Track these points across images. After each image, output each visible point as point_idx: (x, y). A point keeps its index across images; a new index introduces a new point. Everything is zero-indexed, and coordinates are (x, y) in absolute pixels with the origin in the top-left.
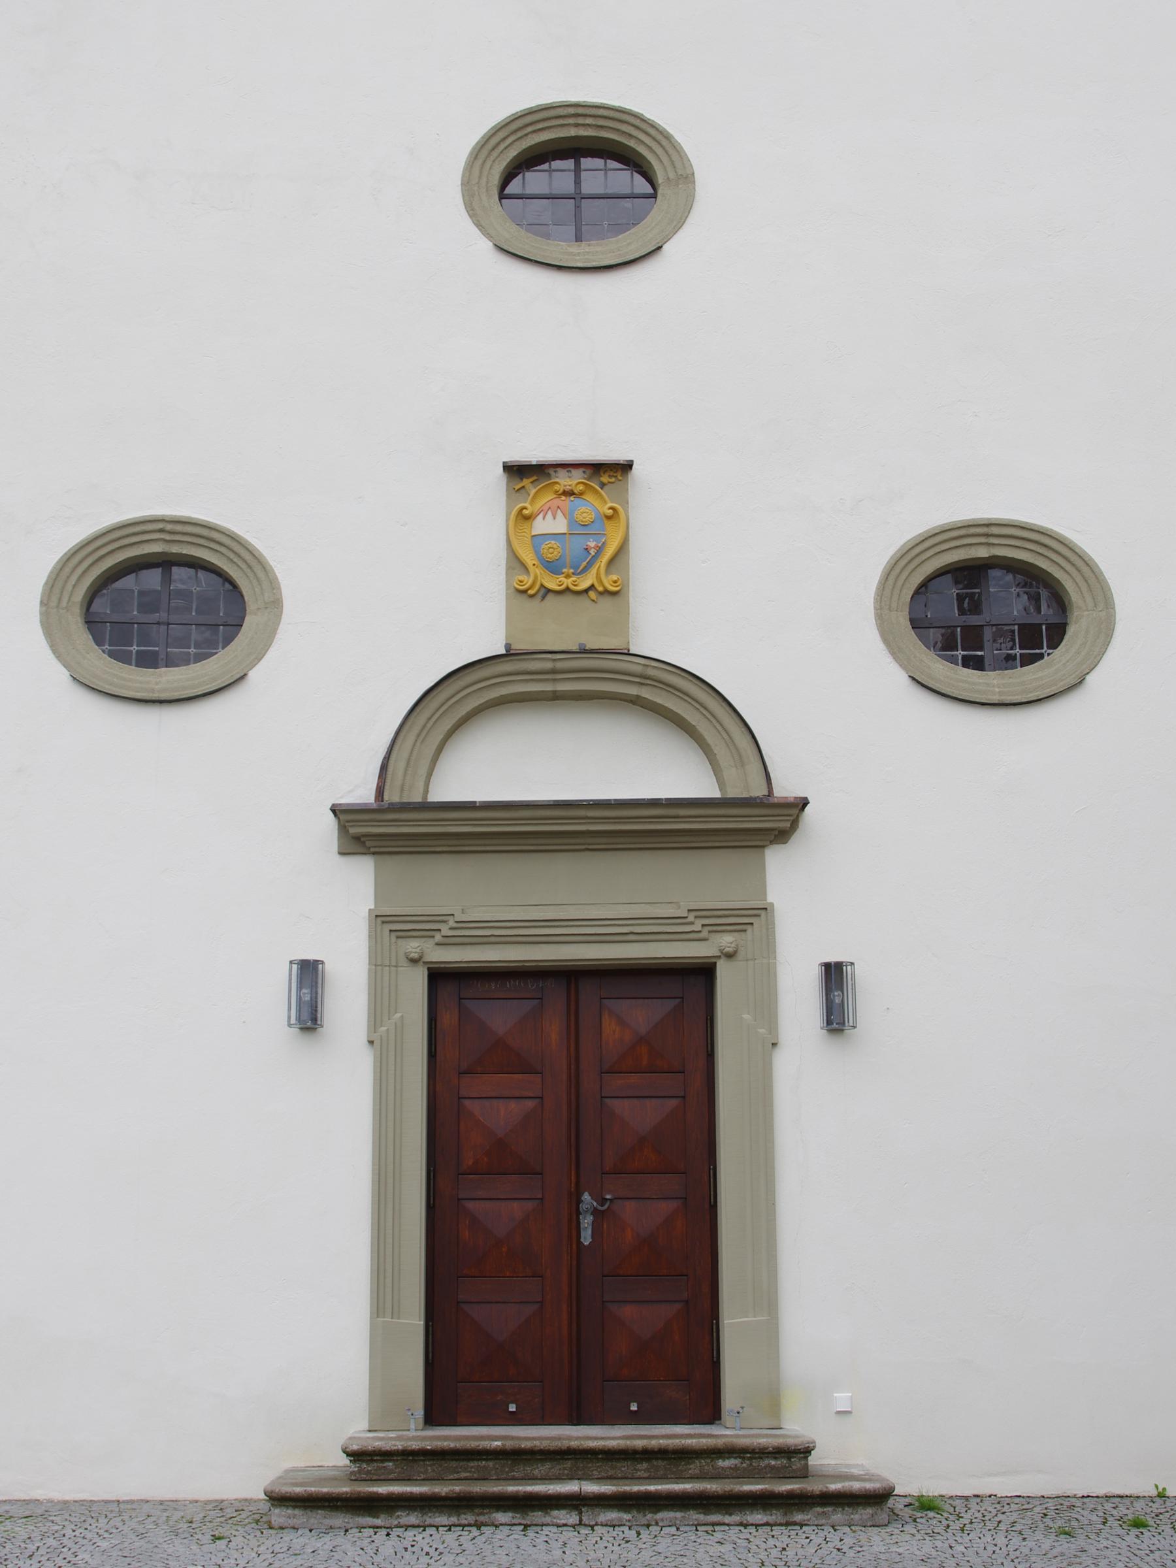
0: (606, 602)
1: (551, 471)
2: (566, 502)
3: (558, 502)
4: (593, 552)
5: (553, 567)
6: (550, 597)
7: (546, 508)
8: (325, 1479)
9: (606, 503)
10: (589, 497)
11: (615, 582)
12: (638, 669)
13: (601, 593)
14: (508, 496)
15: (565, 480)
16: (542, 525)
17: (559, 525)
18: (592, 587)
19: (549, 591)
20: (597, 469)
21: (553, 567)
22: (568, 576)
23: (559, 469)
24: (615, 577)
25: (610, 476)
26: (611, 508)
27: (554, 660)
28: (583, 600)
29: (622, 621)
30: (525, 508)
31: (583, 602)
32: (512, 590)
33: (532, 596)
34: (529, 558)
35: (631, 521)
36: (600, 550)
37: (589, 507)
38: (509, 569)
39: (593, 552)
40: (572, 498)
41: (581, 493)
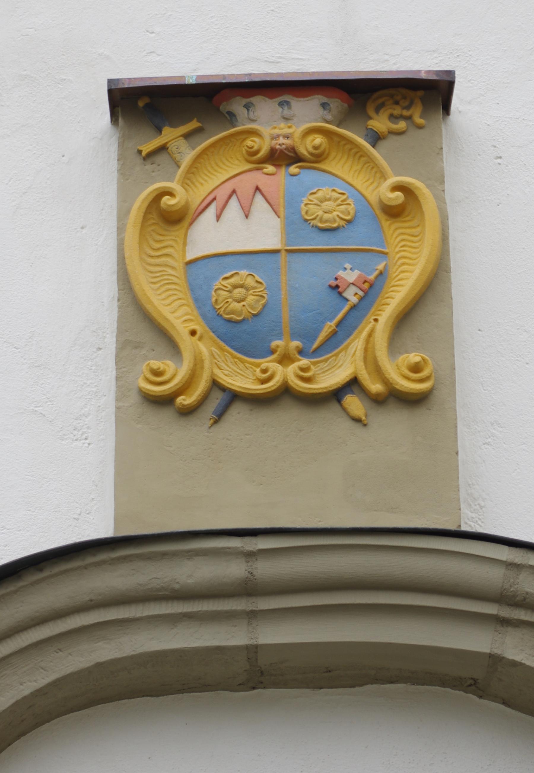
0: (392, 425)
1: (237, 105)
2: (278, 180)
3: (257, 178)
4: (352, 295)
5: (241, 335)
6: (238, 413)
7: (222, 194)
8: (129, 282)
9: (384, 177)
10: (339, 166)
11: (416, 368)
12: (491, 577)
13: (378, 401)
14: (124, 172)
15: (271, 125)
16: (210, 236)
17: (263, 230)
18: (353, 384)
19: (234, 397)
20: (359, 95)
21: (241, 335)
22: (285, 359)
23: (258, 100)
24: (414, 358)
25: (393, 118)
26: (397, 188)
27: (250, 555)
28: (328, 420)
29: (443, 464)
30: (171, 193)
31: (328, 424)
32: (134, 398)
33: (187, 412)
34: (178, 314)
35: (453, 234)
36: (371, 290)
37: (344, 187)
38: (126, 347)
39: (352, 295)
40: (293, 169)
41: (318, 158)
